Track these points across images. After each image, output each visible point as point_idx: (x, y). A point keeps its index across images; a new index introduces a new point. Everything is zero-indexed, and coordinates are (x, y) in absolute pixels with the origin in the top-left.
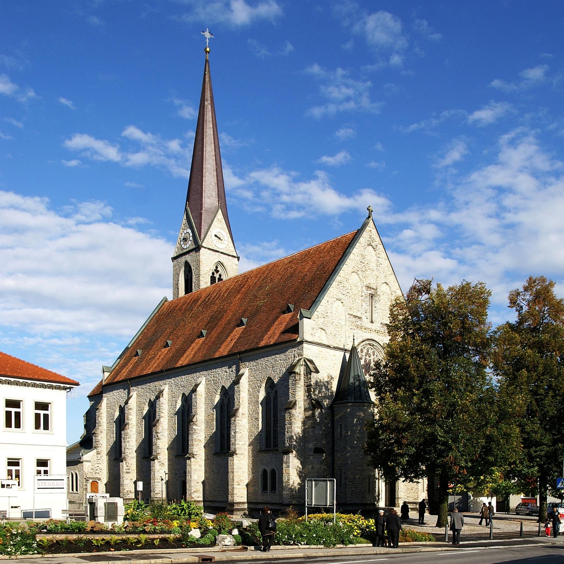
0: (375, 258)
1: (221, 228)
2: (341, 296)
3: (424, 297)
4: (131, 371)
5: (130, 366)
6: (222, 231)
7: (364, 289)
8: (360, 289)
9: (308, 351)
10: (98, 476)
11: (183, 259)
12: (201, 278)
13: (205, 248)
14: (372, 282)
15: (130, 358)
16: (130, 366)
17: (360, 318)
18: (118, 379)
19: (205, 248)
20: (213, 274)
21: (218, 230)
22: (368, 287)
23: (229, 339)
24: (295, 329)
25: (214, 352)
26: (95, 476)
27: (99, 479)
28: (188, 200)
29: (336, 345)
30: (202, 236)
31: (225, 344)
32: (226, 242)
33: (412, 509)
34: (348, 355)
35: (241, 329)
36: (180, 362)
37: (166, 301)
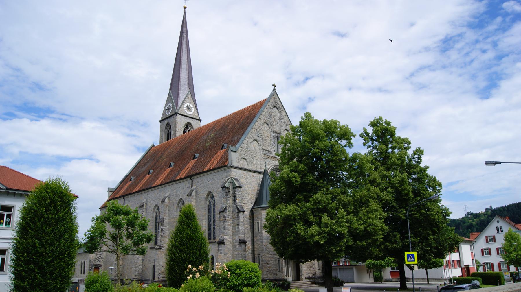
0: (278, 115)
1: (190, 103)
2: (256, 138)
3: (431, 190)
4: (127, 190)
5: (126, 187)
6: (190, 105)
7: (272, 133)
8: (269, 133)
9: (235, 173)
10: (100, 263)
11: (166, 122)
12: (177, 132)
13: (180, 114)
14: (277, 129)
15: (127, 182)
16: (126, 187)
17: (270, 152)
18: (118, 196)
19: (180, 114)
20: (185, 129)
21: (188, 104)
22: (275, 132)
23: (187, 167)
24: (226, 158)
25: (177, 177)
26: (97, 263)
27: (100, 266)
28: (170, 89)
29: (253, 169)
30: (178, 108)
31: (184, 170)
32: (193, 111)
33: (477, 270)
34: (261, 176)
35: (193, 161)
36: (156, 183)
37: (154, 146)
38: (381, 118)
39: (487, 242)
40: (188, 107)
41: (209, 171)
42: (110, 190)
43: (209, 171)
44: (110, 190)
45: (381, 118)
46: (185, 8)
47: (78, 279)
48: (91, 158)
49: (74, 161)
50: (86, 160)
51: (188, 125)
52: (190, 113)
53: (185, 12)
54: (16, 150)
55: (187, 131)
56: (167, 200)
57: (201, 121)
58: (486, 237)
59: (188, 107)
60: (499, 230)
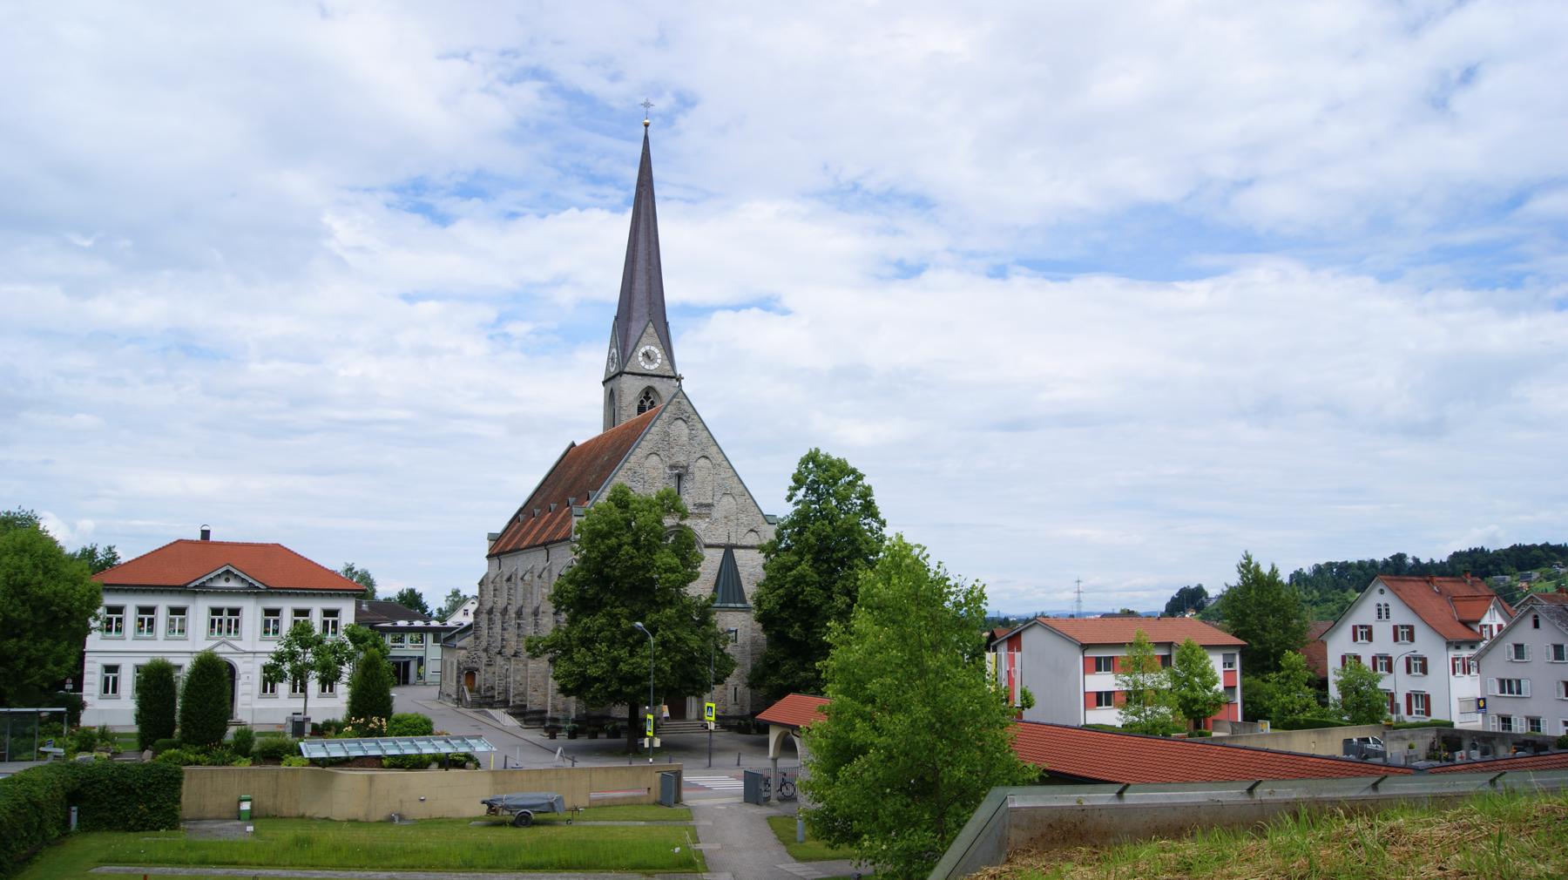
37: (573, 445)
38: (817, 450)
39: (1355, 639)
40: (647, 355)
41: (510, 551)
42: (491, 537)
43: (510, 551)
44: (491, 537)
45: (817, 450)
46: (647, 125)
47: (551, 680)
48: (768, 304)
49: (719, 316)
50: (755, 311)
51: (648, 393)
52: (651, 367)
53: (646, 138)
54: (565, 296)
55: (647, 404)
56: (545, 574)
57: (679, 379)
58: (1355, 628)
59: (647, 355)
60: (1383, 612)
